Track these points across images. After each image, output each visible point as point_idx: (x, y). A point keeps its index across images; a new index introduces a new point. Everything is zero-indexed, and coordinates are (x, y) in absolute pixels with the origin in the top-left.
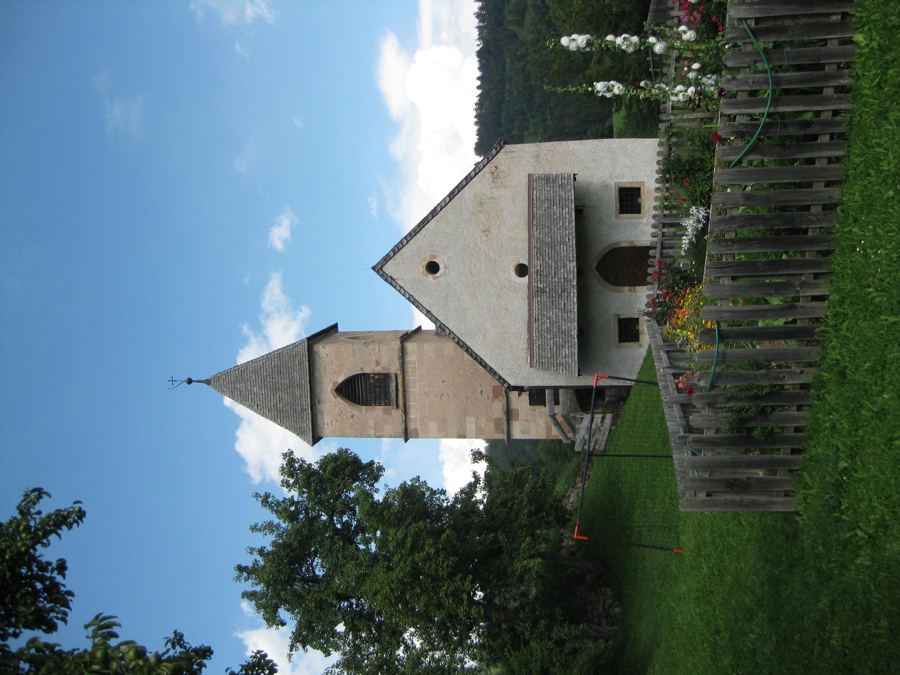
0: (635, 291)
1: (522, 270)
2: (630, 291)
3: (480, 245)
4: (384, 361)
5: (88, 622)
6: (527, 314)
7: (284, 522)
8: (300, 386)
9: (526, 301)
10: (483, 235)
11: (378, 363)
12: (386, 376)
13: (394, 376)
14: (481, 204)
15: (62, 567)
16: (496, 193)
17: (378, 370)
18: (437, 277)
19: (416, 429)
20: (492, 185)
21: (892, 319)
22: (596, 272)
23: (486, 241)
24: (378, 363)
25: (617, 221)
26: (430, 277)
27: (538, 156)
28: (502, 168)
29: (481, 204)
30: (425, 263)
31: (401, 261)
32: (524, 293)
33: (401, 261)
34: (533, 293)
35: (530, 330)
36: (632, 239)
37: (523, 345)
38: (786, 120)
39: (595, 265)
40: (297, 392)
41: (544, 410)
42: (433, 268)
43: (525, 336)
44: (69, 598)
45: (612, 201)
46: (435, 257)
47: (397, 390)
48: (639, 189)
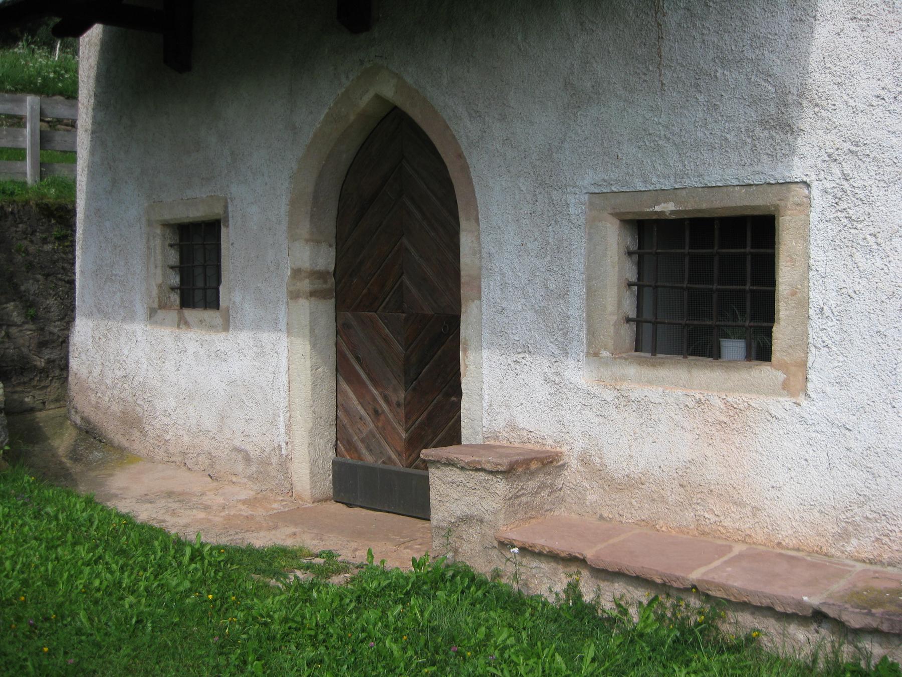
0: (294, 296)
2: (297, 273)
7: (48, 309)
21: (30, 668)
22: (365, 100)
25: (576, 205)
36: (490, 289)
38: (466, 603)
39: (389, 91)
41: (776, 541)
45: (707, 174)
48: (761, 352)
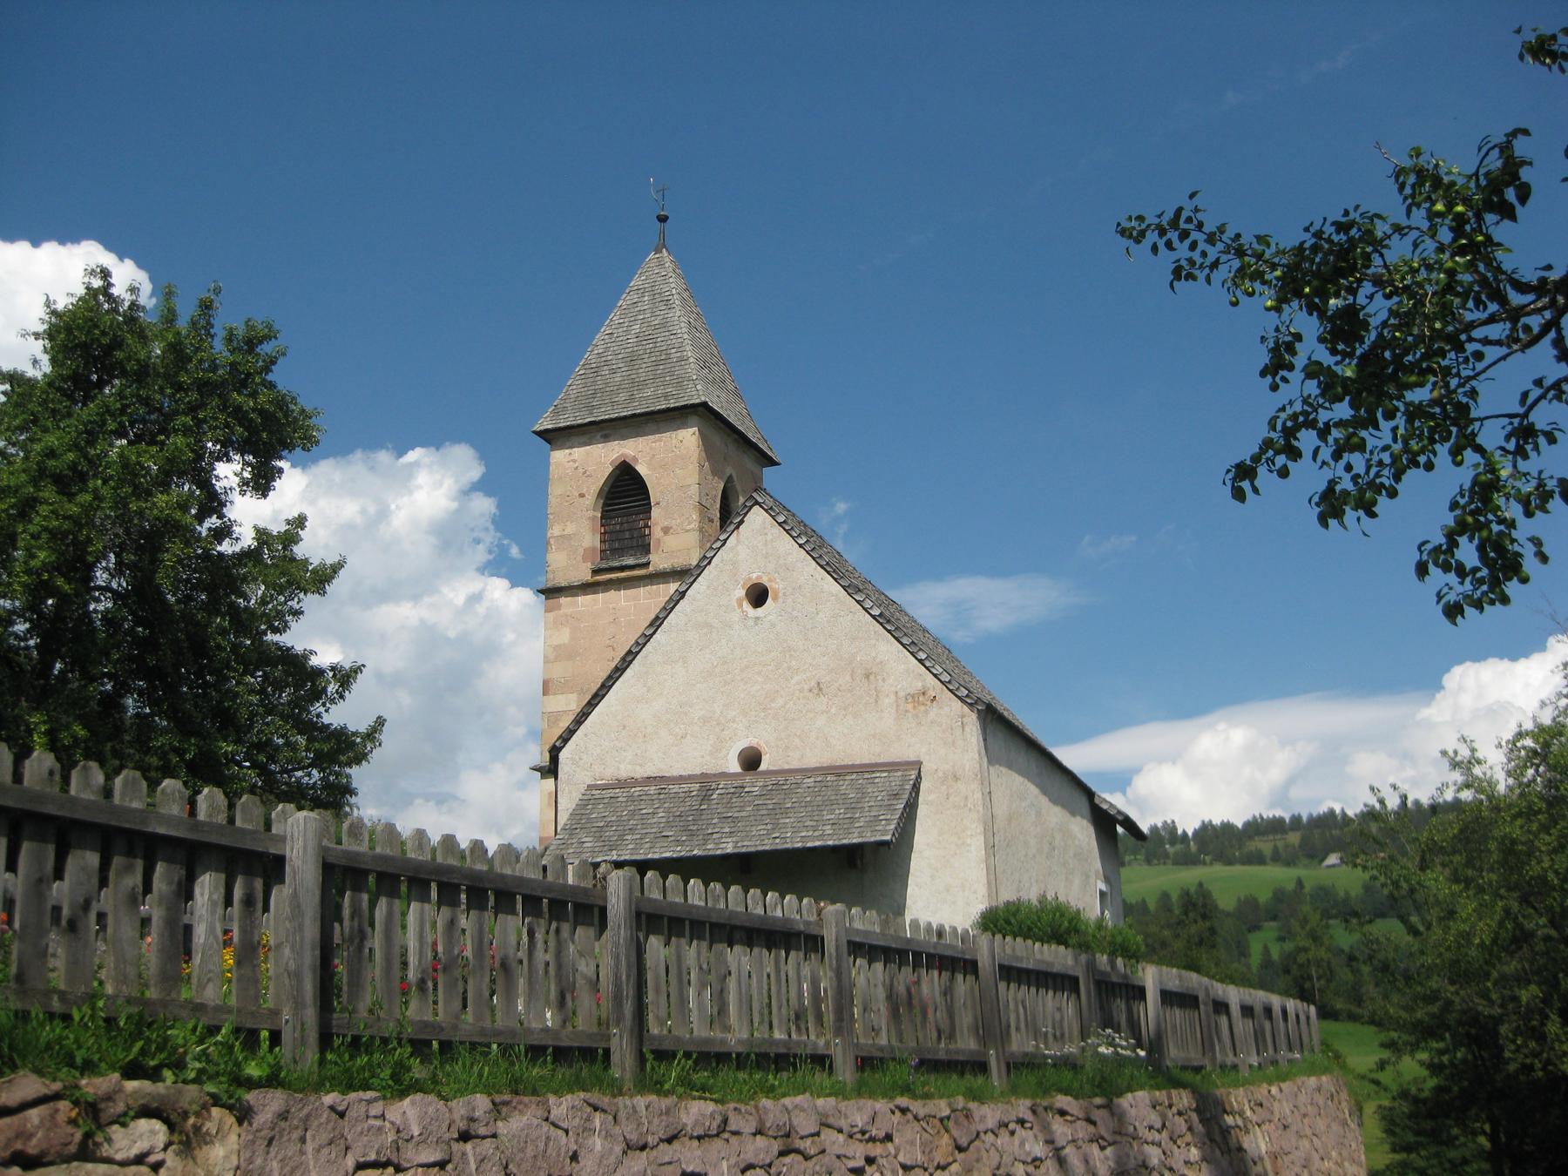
1: (751, 761)
3: (796, 678)
4: (670, 542)
5: (1245, 454)
6: (675, 773)
8: (632, 398)
9: (698, 771)
10: (813, 683)
11: (666, 530)
12: (646, 549)
13: (644, 560)
14: (867, 676)
15: (1429, 467)
16: (888, 701)
17: (657, 532)
18: (741, 606)
19: (559, 607)
20: (902, 694)
23: (801, 691)
24: (666, 530)
26: (741, 592)
27: (956, 778)
28: (934, 711)
29: (867, 676)
30: (765, 581)
31: (769, 537)
32: (711, 767)
33: (769, 537)
34: (706, 782)
35: (649, 780)
37: (625, 771)
40: (622, 397)
42: (758, 596)
43: (640, 772)
44: (1429, 497)
46: (775, 599)
47: (622, 568)
